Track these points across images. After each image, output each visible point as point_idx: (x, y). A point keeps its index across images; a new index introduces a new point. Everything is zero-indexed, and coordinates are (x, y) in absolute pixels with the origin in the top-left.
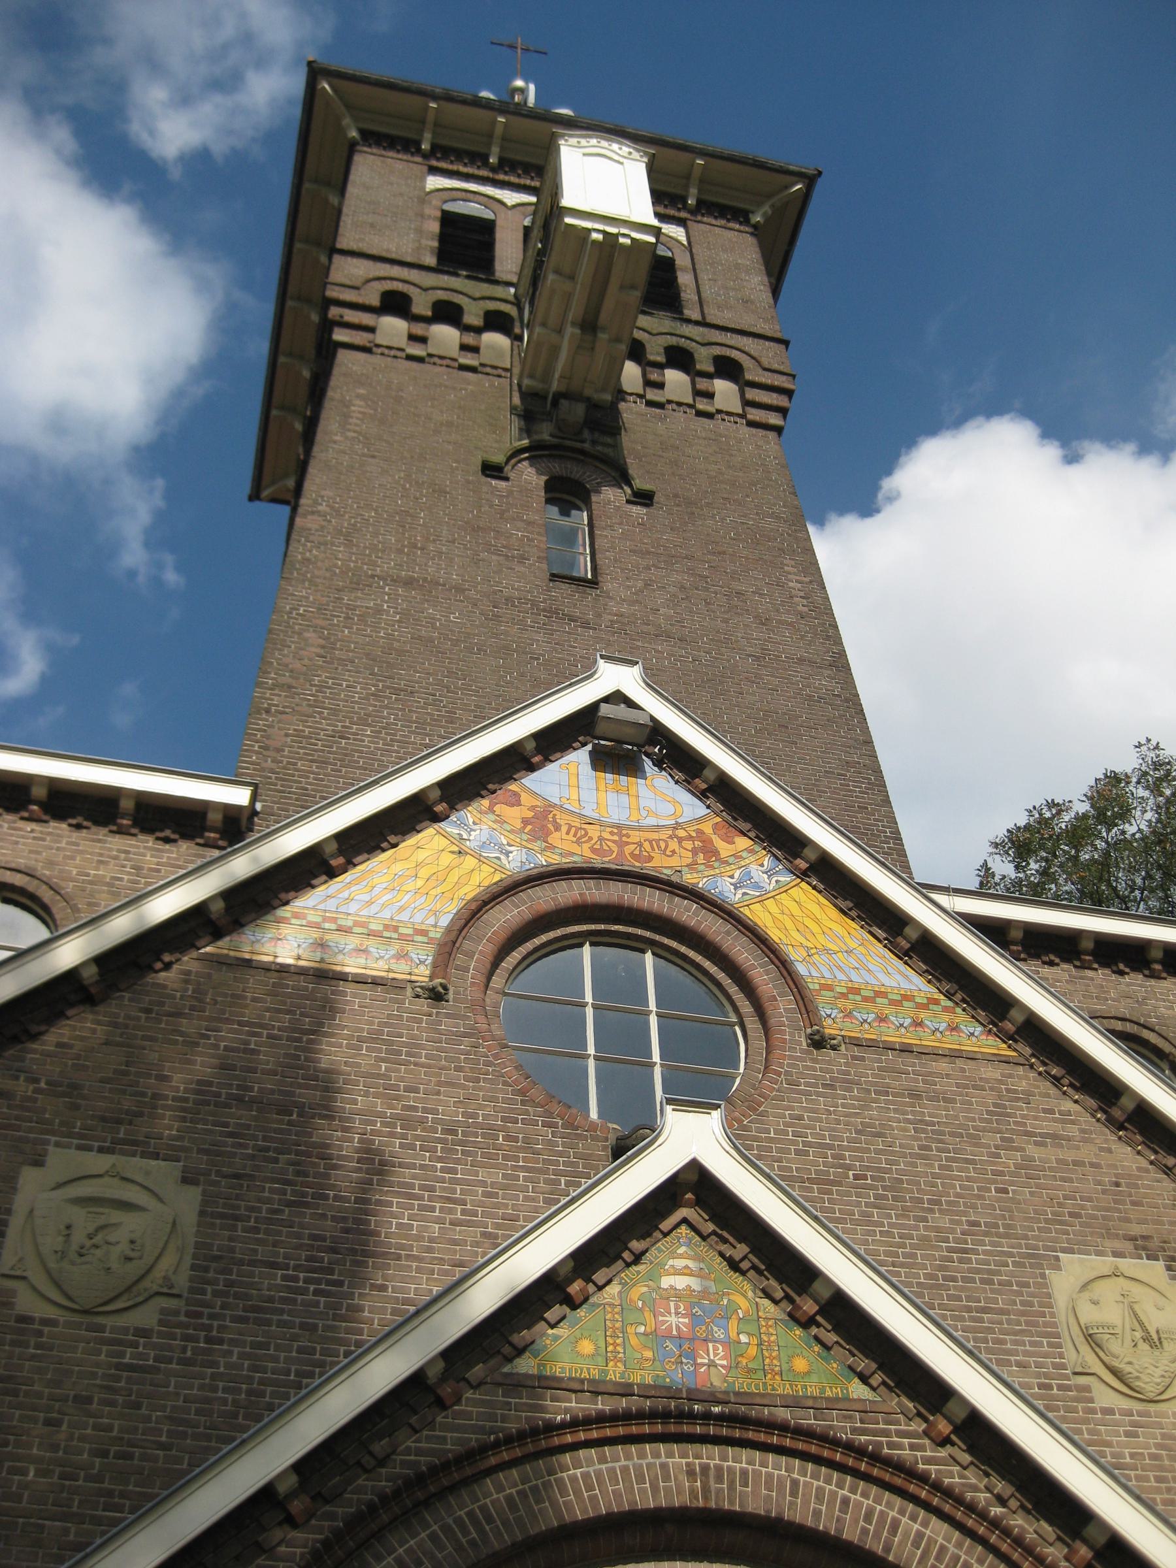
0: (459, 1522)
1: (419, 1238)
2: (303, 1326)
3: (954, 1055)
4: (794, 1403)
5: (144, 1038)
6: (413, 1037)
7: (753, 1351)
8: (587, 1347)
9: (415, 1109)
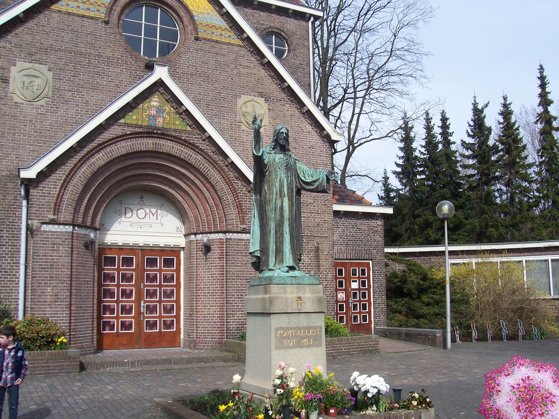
0: (108, 152)
1: (101, 85)
2: (76, 105)
3: (228, 44)
4: (175, 131)
5: (36, 32)
6: (100, 33)
7: (168, 119)
8: (134, 117)
9: (100, 53)
